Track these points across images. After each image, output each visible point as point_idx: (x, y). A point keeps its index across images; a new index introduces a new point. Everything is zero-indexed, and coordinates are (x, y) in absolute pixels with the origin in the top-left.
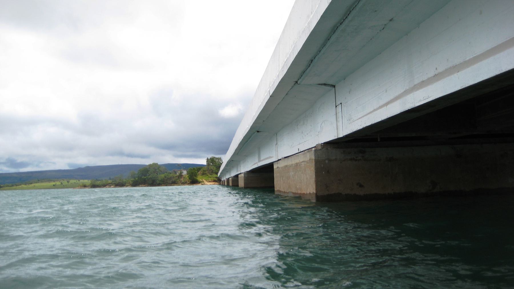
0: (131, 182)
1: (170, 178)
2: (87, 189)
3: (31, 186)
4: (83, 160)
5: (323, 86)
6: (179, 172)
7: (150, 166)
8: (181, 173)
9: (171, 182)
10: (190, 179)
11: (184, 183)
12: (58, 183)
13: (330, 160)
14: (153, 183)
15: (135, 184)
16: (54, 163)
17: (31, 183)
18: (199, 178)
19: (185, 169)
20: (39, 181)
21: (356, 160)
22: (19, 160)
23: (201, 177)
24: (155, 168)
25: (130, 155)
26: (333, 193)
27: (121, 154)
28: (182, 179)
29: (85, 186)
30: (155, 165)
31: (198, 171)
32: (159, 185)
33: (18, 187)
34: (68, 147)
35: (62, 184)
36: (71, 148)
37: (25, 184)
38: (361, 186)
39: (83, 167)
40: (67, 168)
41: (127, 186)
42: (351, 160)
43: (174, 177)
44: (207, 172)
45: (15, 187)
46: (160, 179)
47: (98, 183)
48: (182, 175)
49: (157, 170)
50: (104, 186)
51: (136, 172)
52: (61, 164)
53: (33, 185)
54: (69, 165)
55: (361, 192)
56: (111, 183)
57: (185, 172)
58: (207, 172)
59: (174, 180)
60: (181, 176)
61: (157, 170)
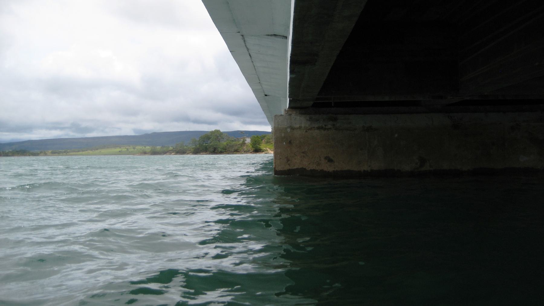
0: (192, 150)
1: (232, 146)
2: (146, 157)
3: (97, 151)
4: (149, 126)
5: (273, 37)
6: (242, 140)
7: (212, 132)
8: (244, 141)
9: (233, 150)
10: (253, 147)
11: (246, 152)
12: (124, 150)
13: (293, 129)
14: (215, 151)
15: (196, 152)
16: (120, 129)
17: (97, 149)
18: (263, 146)
19: (248, 137)
20: (104, 147)
21: (325, 129)
22: (84, 125)
23: (265, 145)
24: (217, 135)
25: (197, 121)
26: (295, 168)
27: (187, 119)
28: (245, 148)
29: (145, 153)
30: (217, 131)
31: (262, 140)
32: (221, 153)
33: (84, 152)
34: (131, 113)
35: (127, 150)
36: (135, 113)
37: (92, 150)
38: (330, 160)
39: (150, 133)
40: (133, 134)
41: (188, 154)
42: (319, 128)
43: (236, 145)
44: (271, 140)
45: (81, 153)
46: (222, 147)
47: (158, 148)
48: (245, 143)
49: (219, 138)
50: (164, 153)
51: (198, 139)
52: (127, 129)
53: (99, 151)
54: (135, 130)
55: (328, 168)
56: (172, 150)
57: (248, 140)
58: (271, 140)
59: (236, 148)
60: (244, 143)
61: (219, 138)
